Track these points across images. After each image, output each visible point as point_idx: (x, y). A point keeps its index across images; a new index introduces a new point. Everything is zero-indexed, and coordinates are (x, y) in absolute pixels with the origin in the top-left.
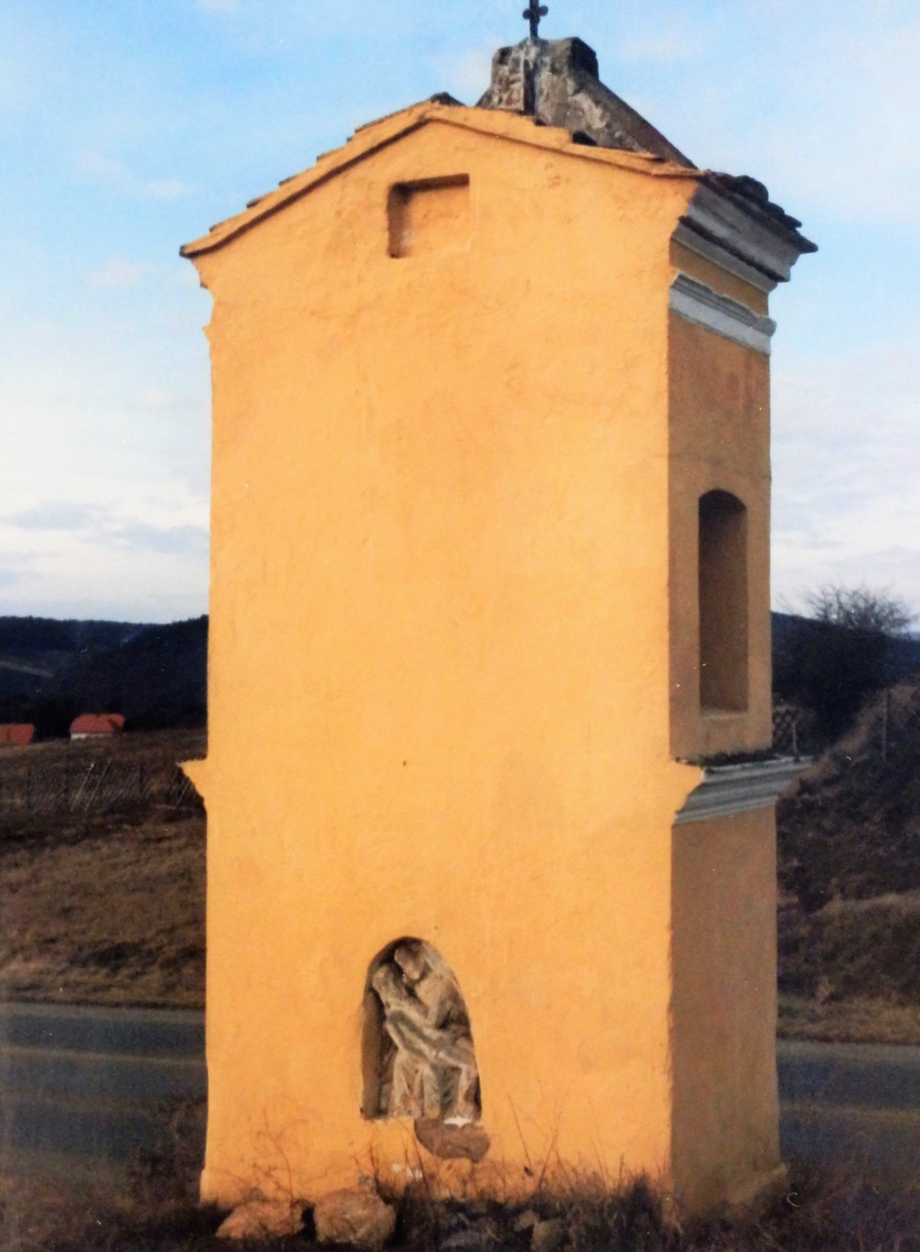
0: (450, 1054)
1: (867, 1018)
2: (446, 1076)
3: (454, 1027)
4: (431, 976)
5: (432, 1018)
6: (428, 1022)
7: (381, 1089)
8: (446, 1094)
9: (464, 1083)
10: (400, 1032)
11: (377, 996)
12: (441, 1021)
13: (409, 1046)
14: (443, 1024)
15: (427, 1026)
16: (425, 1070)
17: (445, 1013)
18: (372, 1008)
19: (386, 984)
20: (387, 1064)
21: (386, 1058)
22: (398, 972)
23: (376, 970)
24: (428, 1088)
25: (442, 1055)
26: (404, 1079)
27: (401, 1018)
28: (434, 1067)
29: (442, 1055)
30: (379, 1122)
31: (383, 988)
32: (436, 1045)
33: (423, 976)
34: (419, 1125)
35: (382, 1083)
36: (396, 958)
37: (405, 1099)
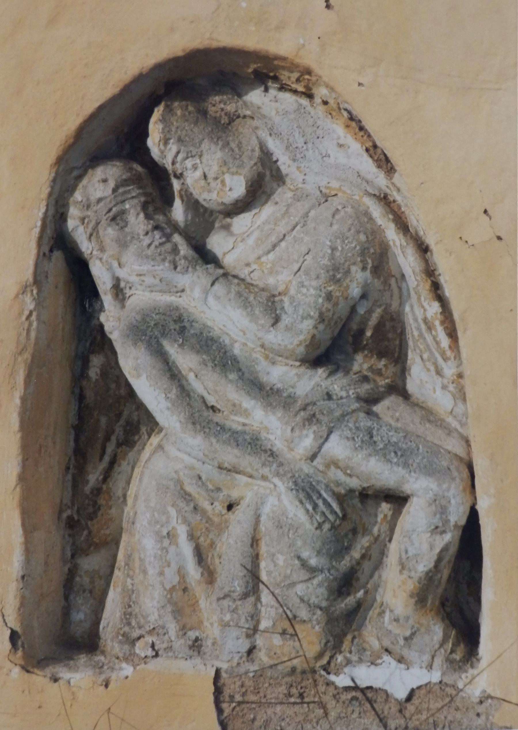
0: (369, 440)
1: (346, 705)
2: (355, 515)
3: (361, 363)
4: (283, 195)
5: (299, 328)
6: (275, 338)
7: (72, 574)
8: (345, 584)
9: (416, 543)
10: (173, 374)
11: (78, 270)
12: (326, 337)
13: (202, 416)
14: (326, 354)
15: (273, 354)
16: (276, 501)
17: (343, 309)
18: (59, 301)
19: (118, 218)
20: (97, 491)
21: (93, 477)
22: (156, 185)
23: (96, 159)
24: (274, 566)
25: (337, 447)
26: (182, 531)
27: (164, 328)
28: (306, 490)
29: (337, 447)
30: (79, 676)
31: (109, 233)
32: (308, 413)
33: (256, 194)
34: (231, 687)
35: (77, 552)
36: (153, 142)
37: (181, 602)
